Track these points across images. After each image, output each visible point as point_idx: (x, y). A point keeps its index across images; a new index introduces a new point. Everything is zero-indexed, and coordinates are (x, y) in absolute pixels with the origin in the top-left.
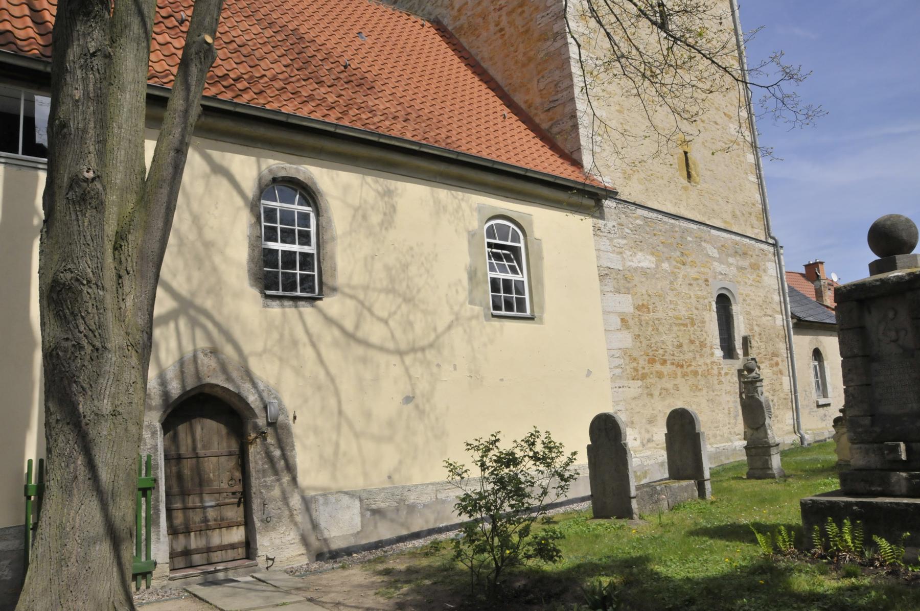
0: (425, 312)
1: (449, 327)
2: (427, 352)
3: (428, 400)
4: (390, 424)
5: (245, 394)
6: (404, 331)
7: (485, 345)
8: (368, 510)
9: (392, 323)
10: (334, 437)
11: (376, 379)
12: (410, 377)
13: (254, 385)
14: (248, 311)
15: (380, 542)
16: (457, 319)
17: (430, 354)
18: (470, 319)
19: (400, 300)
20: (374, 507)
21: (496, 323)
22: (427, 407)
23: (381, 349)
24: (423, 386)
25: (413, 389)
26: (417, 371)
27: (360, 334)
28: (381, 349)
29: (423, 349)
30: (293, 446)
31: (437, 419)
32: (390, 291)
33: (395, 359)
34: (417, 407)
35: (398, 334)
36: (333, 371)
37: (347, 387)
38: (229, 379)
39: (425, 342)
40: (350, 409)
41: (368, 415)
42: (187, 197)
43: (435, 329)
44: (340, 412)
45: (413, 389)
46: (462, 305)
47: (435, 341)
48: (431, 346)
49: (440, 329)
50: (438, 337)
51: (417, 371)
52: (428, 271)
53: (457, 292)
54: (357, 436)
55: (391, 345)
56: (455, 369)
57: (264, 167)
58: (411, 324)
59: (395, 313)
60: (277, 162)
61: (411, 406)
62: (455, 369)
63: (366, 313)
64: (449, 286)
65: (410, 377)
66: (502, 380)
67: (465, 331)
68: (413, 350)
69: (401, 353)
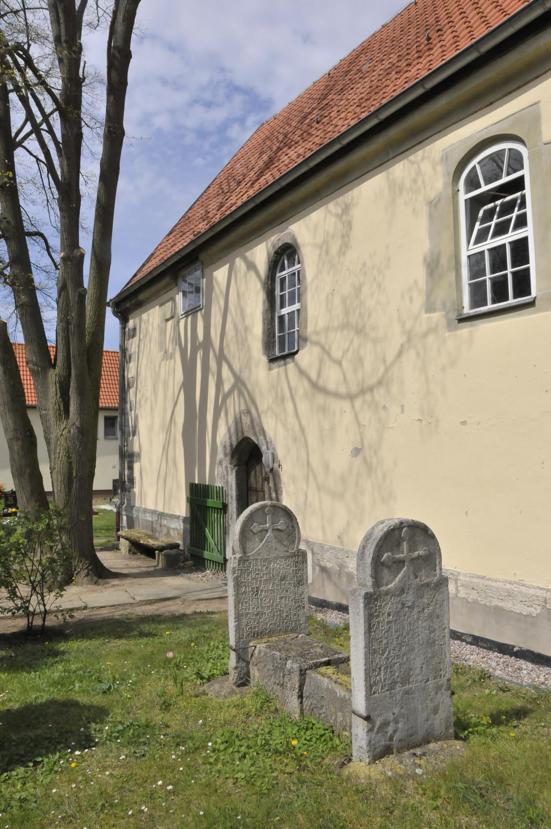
0: (375, 341)
1: (400, 353)
2: (375, 392)
3: (376, 453)
4: (343, 479)
5: (260, 445)
6: (355, 371)
7: (443, 369)
8: (318, 565)
9: (345, 364)
10: (305, 487)
11: (332, 428)
12: (359, 424)
13: (265, 436)
14: (261, 374)
15: (325, 601)
16: (409, 340)
17: (379, 395)
18: (425, 335)
19: (352, 333)
20: (322, 564)
21: (465, 330)
22: (374, 461)
23: (336, 395)
24: (371, 434)
25: (362, 440)
26: (366, 417)
27: (321, 383)
28: (336, 395)
29: (371, 389)
30: (282, 491)
31: (384, 476)
32: (345, 326)
33: (346, 405)
34: (365, 460)
35: (350, 376)
36: (304, 423)
37: (312, 438)
38: (255, 434)
39: (372, 381)
40: (315, 461)
41: (326, 467)
42: (217, 282)
43: (384, 361)
44: (308, 463)
45: (362, 440)
46: (416, 318)
47: (383, 376)
48: (380, 383)
49: (390, 359)
50: (387, 370)
51: (366, 417)
52: (379, 285)
53: (411, 300)
54: (319, 488)
55: (343, 390)
56: (402, 411)
57: (270, 244)
58: (360, 360)
59: (348, 350)
60: (275, 236)
61: (359, 459)
62: (402, 411)
63: (326, 358)
64: (403, 296)
65: (359, 424)
66: (464, 423)
67: (418, 355)
68: (363, 392)
69: (351, 397)
